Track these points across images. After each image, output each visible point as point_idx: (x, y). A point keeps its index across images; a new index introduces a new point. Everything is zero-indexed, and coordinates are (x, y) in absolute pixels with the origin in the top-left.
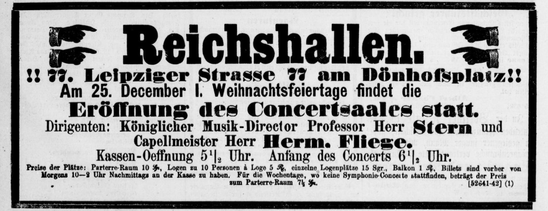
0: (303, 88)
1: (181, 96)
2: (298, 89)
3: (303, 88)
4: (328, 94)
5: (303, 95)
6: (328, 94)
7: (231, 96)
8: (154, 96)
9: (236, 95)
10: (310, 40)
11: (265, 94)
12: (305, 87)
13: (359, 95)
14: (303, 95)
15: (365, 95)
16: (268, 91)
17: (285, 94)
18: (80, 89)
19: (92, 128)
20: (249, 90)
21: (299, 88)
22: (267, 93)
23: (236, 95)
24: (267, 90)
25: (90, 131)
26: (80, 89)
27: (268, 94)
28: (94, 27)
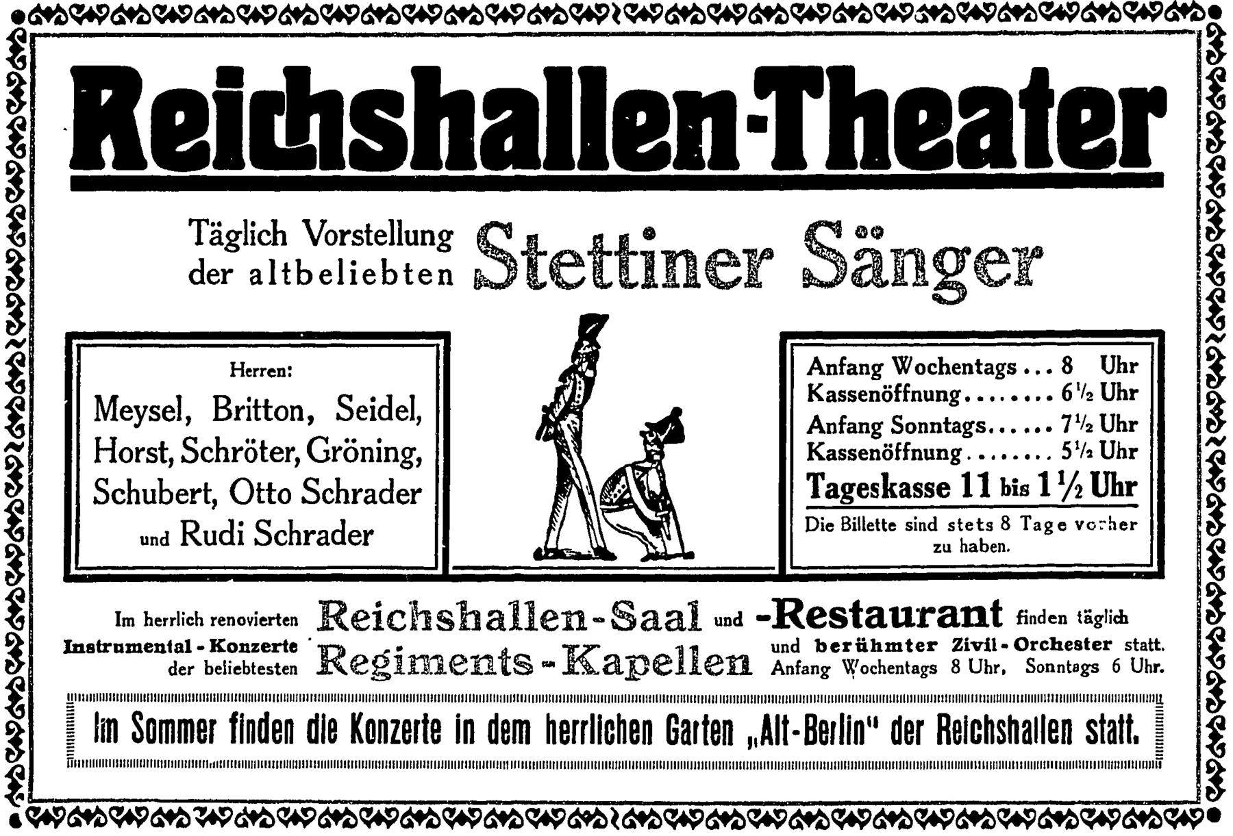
13: (940, 742)
20: (313, 737)
22: (979, 736)
24: (980, 728)
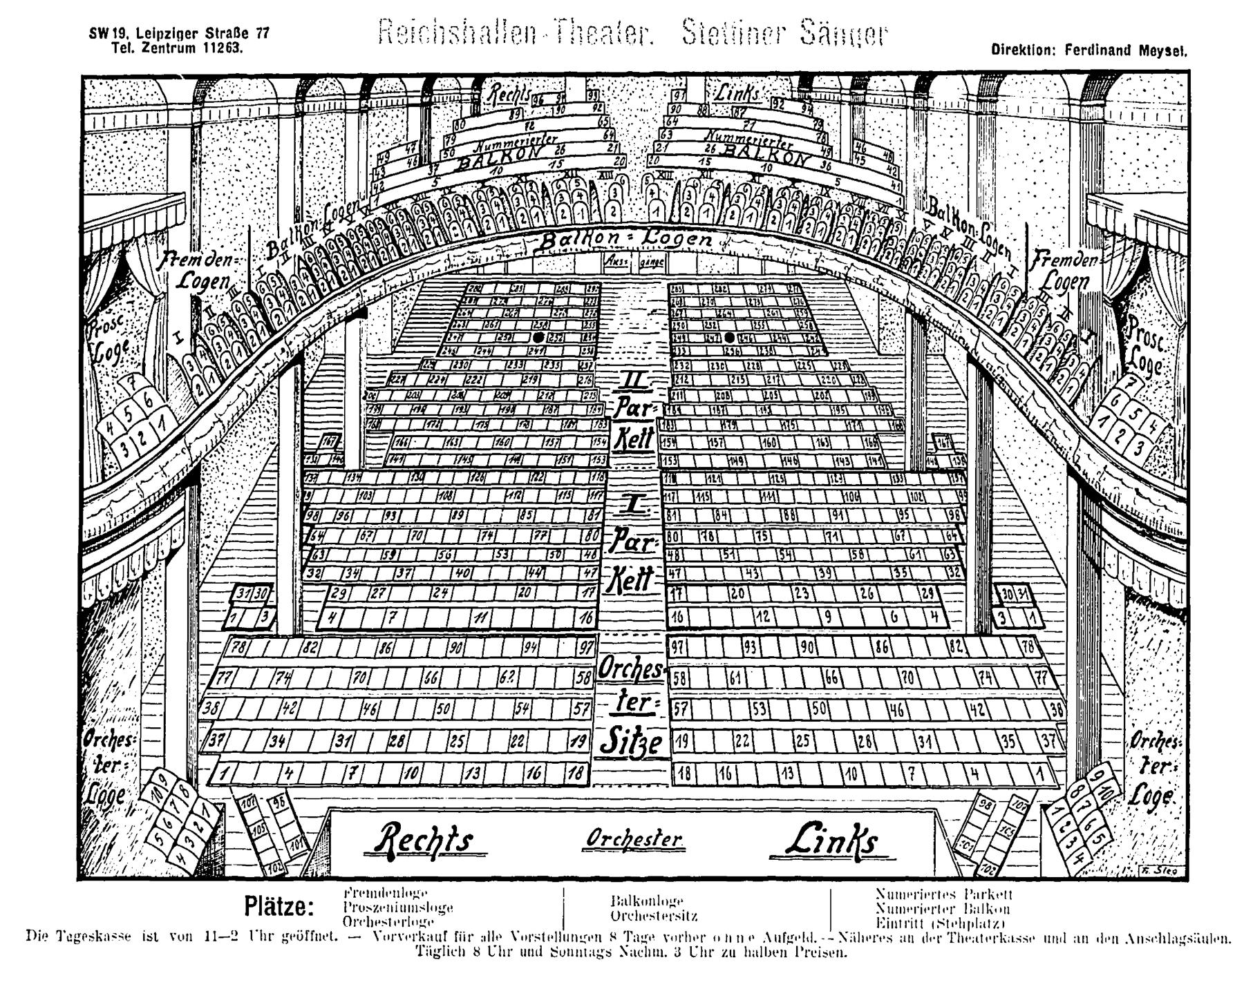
13: (683, 849)
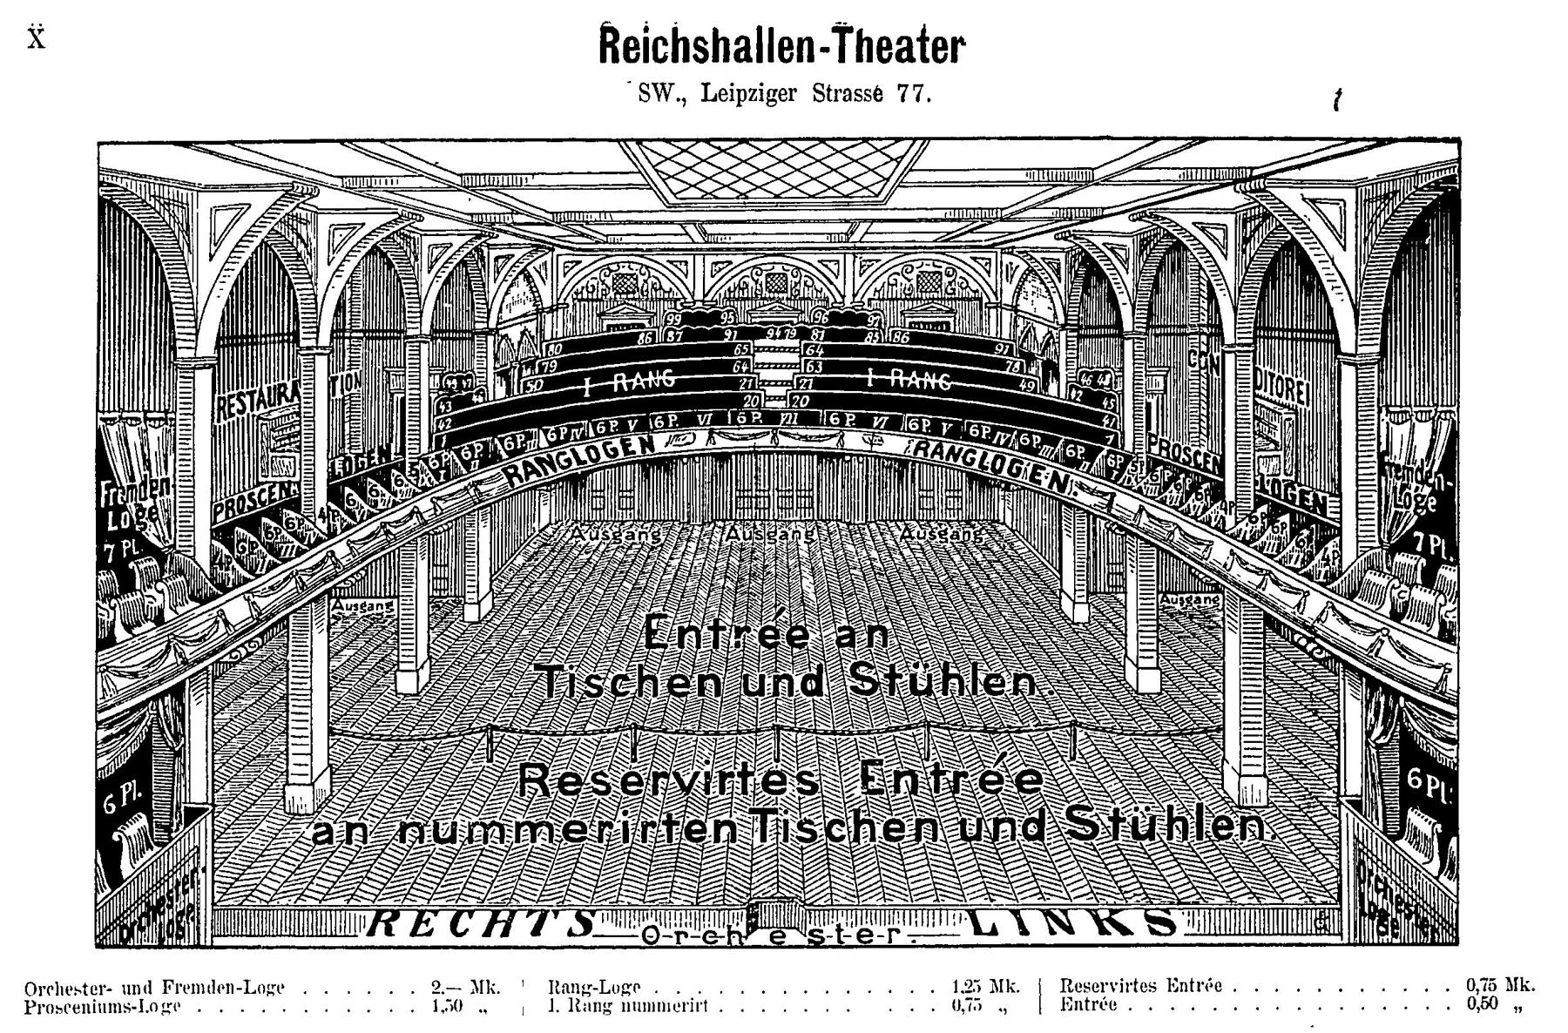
0: (646, 40)
1: (954, 59)
2: (940, 44)
3: (646, 40)
4: (742, 55)
5: (646, 60)
6: (742, 55)
7: (635, 60)
8: (800, 59)
9: (716, 59)
10: (899, 42)
11: (660, 56)
12: (652, 36)
13: (603, 59)
14: (646, 60)
15: (865, 57)
16: (669, 49)
17: (701, 56)
18: (1457, 944)
19: (929, 54)
20: (806, 44)
21: (635, 40)
23: (800, 59)
25: (925, 60)
26: (1457, 944)
27: (670, 56)
28: (939, 29)
